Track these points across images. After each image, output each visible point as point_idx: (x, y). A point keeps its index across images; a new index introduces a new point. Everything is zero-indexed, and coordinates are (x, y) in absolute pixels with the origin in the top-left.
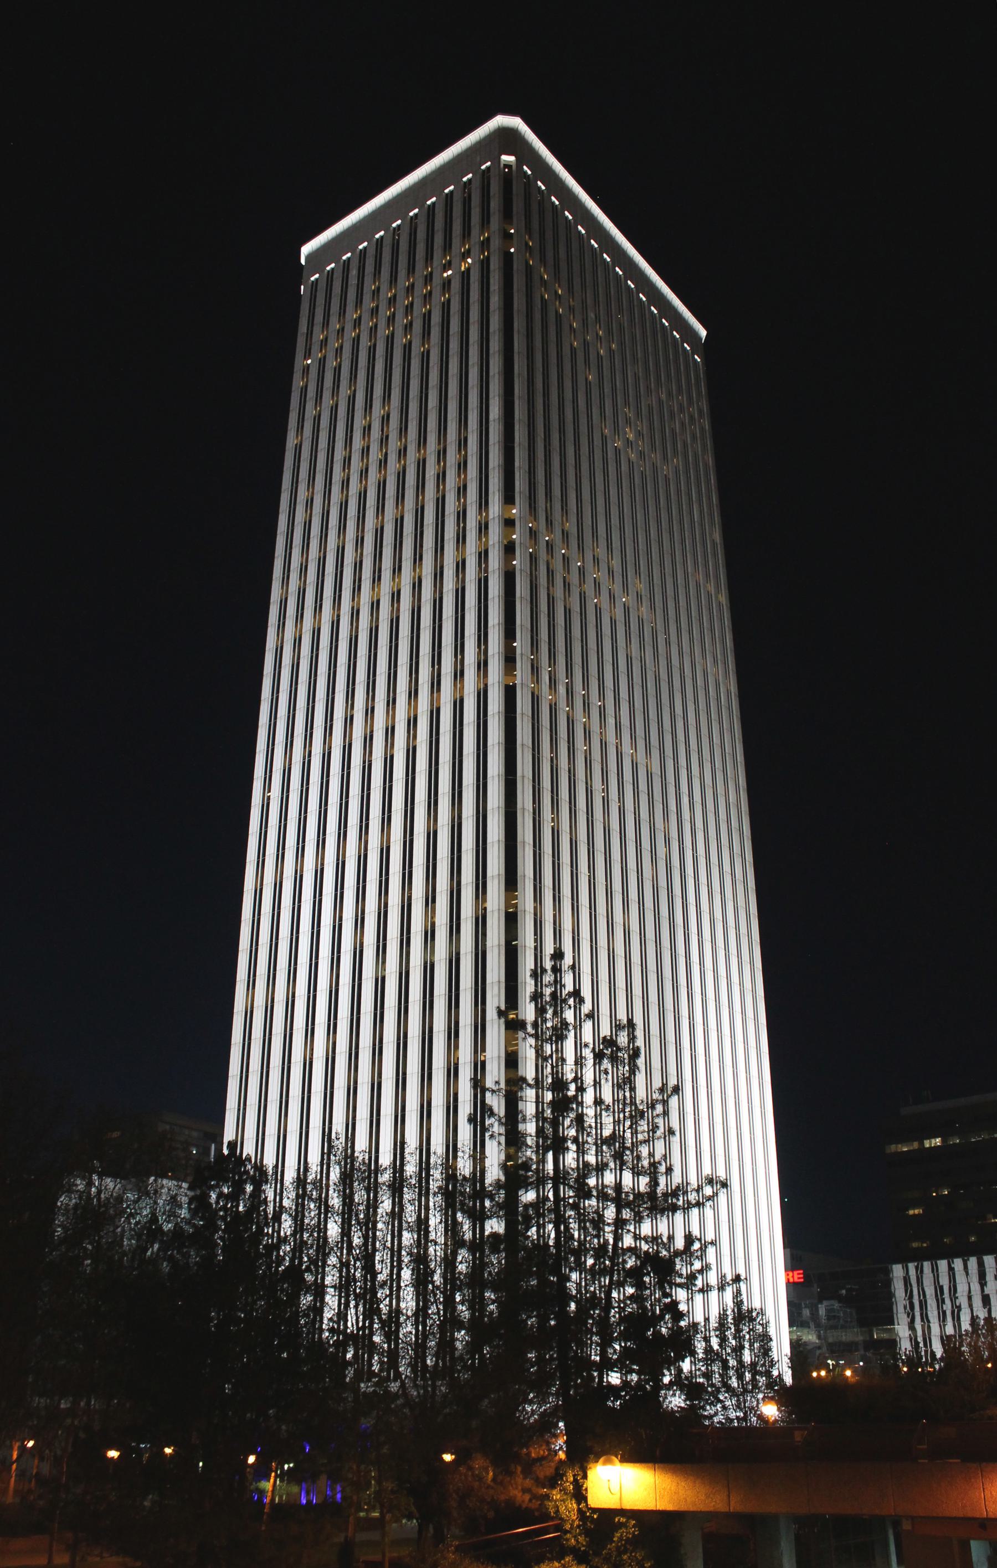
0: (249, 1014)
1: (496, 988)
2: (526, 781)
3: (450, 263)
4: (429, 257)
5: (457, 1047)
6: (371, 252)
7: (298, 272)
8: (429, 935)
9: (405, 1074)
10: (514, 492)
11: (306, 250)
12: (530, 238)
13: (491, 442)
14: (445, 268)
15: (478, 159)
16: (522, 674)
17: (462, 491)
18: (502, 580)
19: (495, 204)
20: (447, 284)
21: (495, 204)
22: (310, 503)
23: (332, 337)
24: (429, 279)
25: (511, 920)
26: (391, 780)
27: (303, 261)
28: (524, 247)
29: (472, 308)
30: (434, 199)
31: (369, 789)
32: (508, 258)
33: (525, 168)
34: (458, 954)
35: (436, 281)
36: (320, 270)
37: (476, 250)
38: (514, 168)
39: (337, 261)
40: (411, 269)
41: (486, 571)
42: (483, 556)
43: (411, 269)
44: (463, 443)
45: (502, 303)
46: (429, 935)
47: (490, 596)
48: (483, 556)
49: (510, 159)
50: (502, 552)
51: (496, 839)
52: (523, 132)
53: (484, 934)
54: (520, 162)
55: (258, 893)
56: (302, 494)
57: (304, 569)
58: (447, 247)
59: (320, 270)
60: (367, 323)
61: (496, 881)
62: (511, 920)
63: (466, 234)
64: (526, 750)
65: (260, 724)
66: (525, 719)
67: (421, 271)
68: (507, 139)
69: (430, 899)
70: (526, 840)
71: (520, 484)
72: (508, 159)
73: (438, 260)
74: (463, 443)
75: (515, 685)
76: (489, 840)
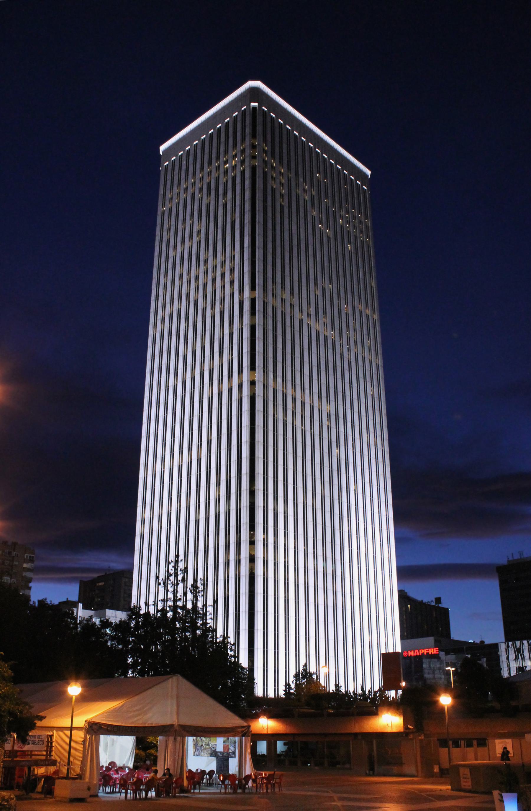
0: (142, 536)
1: (245, 526)
2: (260, 428)
3: (227, 161)
4: (218, 157)
5: (235, 213)
6: (192, 152)
7: (157, 158)
8: (218, 500)
9: (207, 564)
10: (255, 365)
11: (162, 148)
12: (266, 146)
13: (245, 259)
14: (226, 162)
15: (240, 104)
16: (259, 319)
17: (232, 282)
18: (249, 329)
19: (248, 130)
20: (226, 172)
21: (248, 130)
22: (165, 285)
23: (175, 197)
24: (218, 168)
25: (252, 559)
26: (202, 412)
27: (161, 154)
28: (262, 151)
29: (237, 186)
30: (220, 125)
31: (192, 430)
32: (254, 169)
33: (263, 108)
34: (229, 510)
35: (221, 170)
36: (169, 160)
37: (239, 155)
38: (257, 108)
39: (176, 156)
40: (210, 163)
41: (242, 324)
42: (240, 386)
43: (210, 163)
44: (233, 258)
45: (251, 197)
46: (218, 500)
47: (244, 311)
48: (240, 386)
49: (255, 104)
50: (250, 315)
51: (246, 440)
52: (262, 88)
53: (240, 499)
54: (260, 106)
55: (145, 479)
56: (166, 226)
57: (163, 319)
58: (226, 152)
59: (169, 160)
60: (190, 190)
61: (245, 476)
62: (252, 559)
63: (235, 145)
64: (260, 413)
65: (136, 534)
66: (260, 326)
67: (215, 164)
68: (254, 93)
69: (218, 484)
70: (260, 456)
71: (259, 280)
72: (254, 104)
73: (222, 159)
74: (233, 258)
75: (255, 298)
76: (242, 523)
